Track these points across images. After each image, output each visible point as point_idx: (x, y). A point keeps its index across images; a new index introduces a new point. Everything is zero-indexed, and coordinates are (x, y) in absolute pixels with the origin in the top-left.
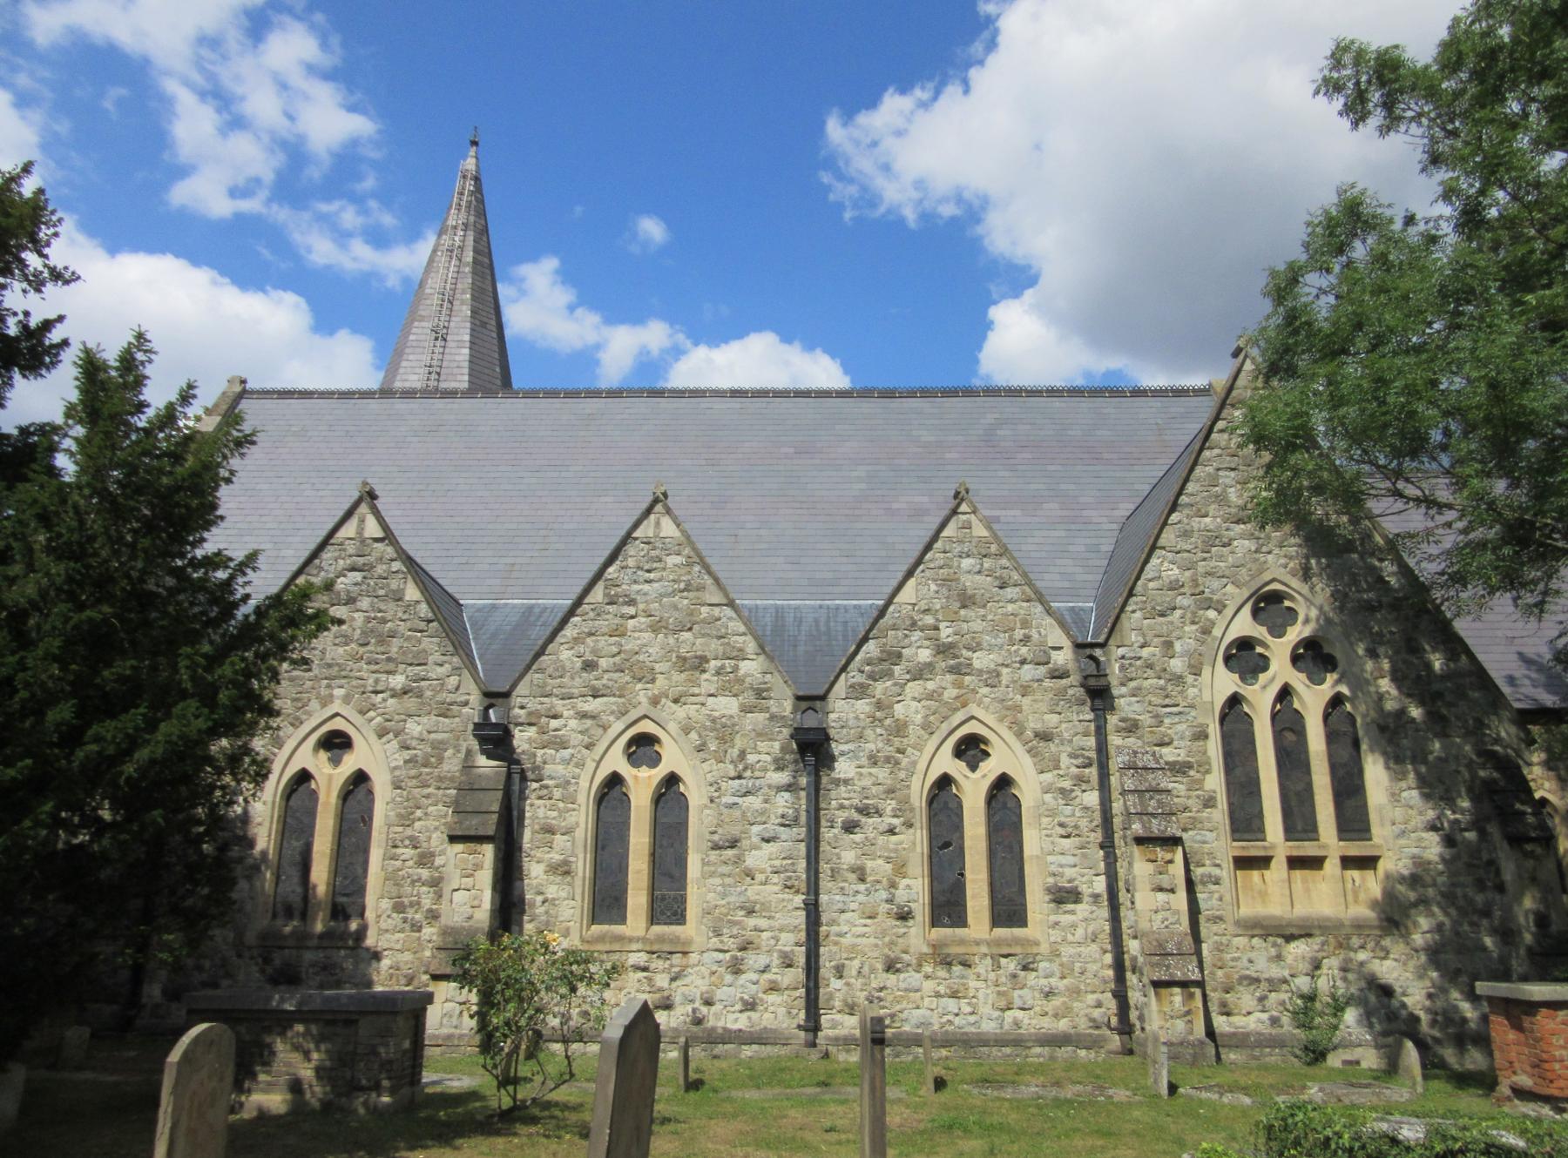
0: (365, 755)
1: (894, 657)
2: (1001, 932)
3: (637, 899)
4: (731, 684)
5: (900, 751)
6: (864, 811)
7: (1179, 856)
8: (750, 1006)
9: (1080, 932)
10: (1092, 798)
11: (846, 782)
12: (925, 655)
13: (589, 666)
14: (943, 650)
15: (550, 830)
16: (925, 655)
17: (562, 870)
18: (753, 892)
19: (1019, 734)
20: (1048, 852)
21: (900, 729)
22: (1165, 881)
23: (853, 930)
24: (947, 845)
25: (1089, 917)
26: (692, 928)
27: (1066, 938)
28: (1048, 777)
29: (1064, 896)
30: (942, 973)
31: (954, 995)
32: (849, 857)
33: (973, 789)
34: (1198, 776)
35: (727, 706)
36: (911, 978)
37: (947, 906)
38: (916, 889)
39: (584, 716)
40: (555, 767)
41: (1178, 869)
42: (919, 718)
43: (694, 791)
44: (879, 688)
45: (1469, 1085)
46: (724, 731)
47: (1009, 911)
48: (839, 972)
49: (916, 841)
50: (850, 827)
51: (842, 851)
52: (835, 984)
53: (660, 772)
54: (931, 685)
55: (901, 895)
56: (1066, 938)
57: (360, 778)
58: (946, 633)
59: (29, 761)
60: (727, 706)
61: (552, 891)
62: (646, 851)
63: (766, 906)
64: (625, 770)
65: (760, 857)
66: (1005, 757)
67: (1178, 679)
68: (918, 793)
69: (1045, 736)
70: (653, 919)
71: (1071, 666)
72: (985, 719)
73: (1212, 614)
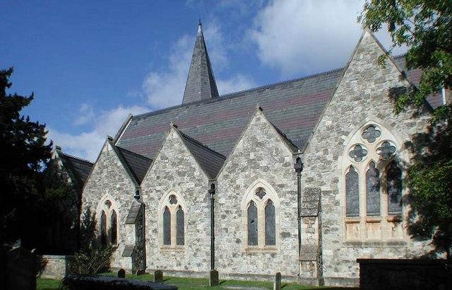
0: (116, 206)
1: (235, 165)
2: (179, 246)
3: (173, 239)
4: (192, 178)
5: (237, 194)
6: (227, 212)
7: (317, 222)
8: (199, 265)
9: (290, 246)
10: (296, 205)
11: (222, 204)
12: (245, 164)
13: (158, 177)
14: (251, 161)
15: (152, 221)
16: (245, 164)
17: (155, 231)
18: (199, 236)
19: (273, 185)
20: (283, 221)
21: (238, 187)
22: (311, 230)
23: (224, 243)
24: (253, 221)
25: (292, 241)
26: (185, 246)
27: (287, 247)
28: (283, 199)
29: (285, 235)
30: (248, 257)
31: (252, 263)
32: (224, 226)
33: (261, 206)
34: (334, 195)
35: (192, 185)
36: (240, 258)
37: (252, 239)
38: (244, 235)
39: (157, 191)
40: (152, 205)
41: (316, 226)
42: (243, 185)
43: (184, 209)
44: (232, 176)
45: (109, 283)
46: (190, 191)
47: (270, 241)
48: (221, 257)
49: (245, 220)
50: (224, 217)
51: (221, 223)
52: (220, 260)
53: (177, 205)
54: (247, 173)
55: (238, 236)
56: (287, 247)
57: (180, 206)
58: (252, 156)
59: (15, 209)
60: (192, 185)
61: (154, 237)
62: (176, 229)
63: (202, 240)
64: (169, 205)
65: (200, 227)
66: (271, 193)
67: (330, 162)
68: (244, 207)
69: (282, 186)
70: (178, 244)
71: (291, 162)
72: (263, 183)
73: (343, 137)
